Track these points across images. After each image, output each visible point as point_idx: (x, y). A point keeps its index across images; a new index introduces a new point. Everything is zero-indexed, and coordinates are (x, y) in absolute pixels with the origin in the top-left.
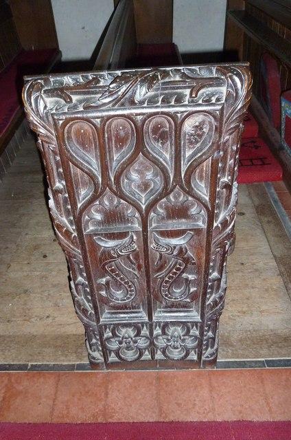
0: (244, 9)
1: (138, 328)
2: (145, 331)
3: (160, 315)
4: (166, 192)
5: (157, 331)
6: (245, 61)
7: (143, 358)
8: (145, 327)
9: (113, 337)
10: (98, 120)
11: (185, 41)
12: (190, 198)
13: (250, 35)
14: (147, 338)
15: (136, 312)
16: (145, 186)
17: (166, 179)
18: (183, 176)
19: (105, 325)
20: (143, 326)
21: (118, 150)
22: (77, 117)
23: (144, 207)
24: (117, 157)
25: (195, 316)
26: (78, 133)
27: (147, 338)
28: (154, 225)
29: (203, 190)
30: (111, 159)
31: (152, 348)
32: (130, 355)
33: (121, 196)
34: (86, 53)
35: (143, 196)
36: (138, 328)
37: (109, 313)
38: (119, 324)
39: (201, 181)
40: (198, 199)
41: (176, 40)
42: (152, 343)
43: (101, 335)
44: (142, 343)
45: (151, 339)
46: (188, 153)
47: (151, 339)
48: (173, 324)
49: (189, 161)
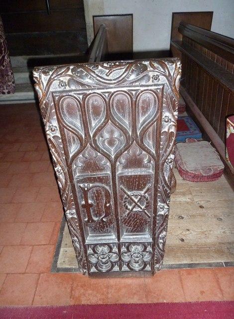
0: (181, 40)
1: (145, 246)
3: (126, 238)
4: (127, 147)
5: (90, 251)
8: (115, 247)
9: (93, 255)
10: (107, 95)
12: (144, 152)
16: (111, 143)
18: (138, 134)
19: (122, 243)
20: (114, 246)
23: (113, 157)
24: (94, 124)
25: (146, 237)
26: (68, 106)
29: (149, 143)
31: (120, 262)
33: (96, 149)
35: (112, 150)
37: (91, 236)
40: (149, 152)
42: (120, 259)
43: (86, 252)
44: (114, 258)
45: (120, 254)
46: (142, 119)
48: (134, 243)
49: (142, 126)
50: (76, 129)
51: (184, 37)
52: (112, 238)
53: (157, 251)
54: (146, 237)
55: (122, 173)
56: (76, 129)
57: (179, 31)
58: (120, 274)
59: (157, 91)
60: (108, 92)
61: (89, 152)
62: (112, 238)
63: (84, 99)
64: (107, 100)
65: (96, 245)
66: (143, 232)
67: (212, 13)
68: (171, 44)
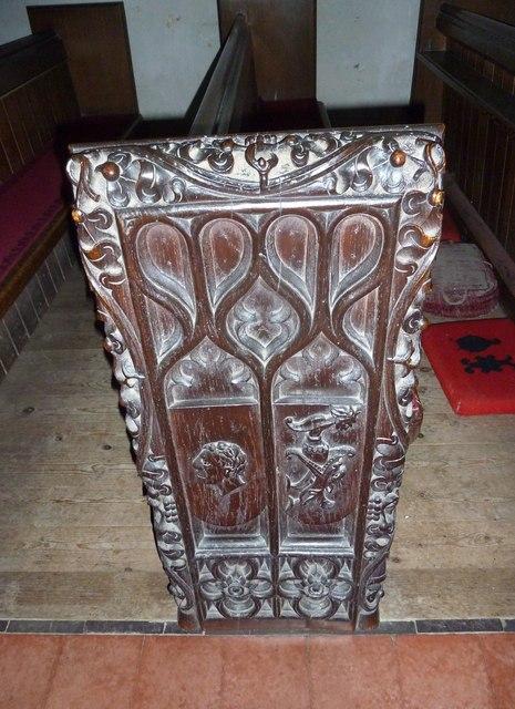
0: (444, 49)
2: (264, 570)
4: (302, 341)
5: (286, 570)
6: (434, 122)
7: (338, 614)
8: (265, 564)
9: (214, 581)
10: (257, 217)
11: (333, 89)
12: (343, 354)
13: (452, 84)
14: (268, 580)
15: (248, 539)
17: (304, 319)
18: (331, 309)
19: (202, 560)
21: (297, 266)
22: (218, 212)
23: (265, 364)
25: (344, 546)
26: (219, 240)
27: (268, 580)
28: (281, 397)
29: (363, 340)
30: (335, 277)
31: (276, 596)
32: (318, 609)
33: (225, 344)
34: (178, 106)
36: (251, 562)
37: (211, 539)
38: (226, 558)
39: (358, 326)
40: (363, 360)
41: (320, 97)
43: (195, 576)
44: (261, 590)
45: (275, 580)
47: (275, 580)
50: (178, 299)
51: (452, 41)
52: (259, 544)
53: (368, 574)
54: (344, 546)
55: (285, 401)
56: (178, 299)
57: (438, 26)
58: (277, 622)
59: (322, 218)
60: (190, 214)
61: (206, 357)
62: (259, 544)
63: (196, 229)
64: (390, 222)
65: (220, 560)
66: (331, 531)
67: (31, 10)
68: (416, 60)
